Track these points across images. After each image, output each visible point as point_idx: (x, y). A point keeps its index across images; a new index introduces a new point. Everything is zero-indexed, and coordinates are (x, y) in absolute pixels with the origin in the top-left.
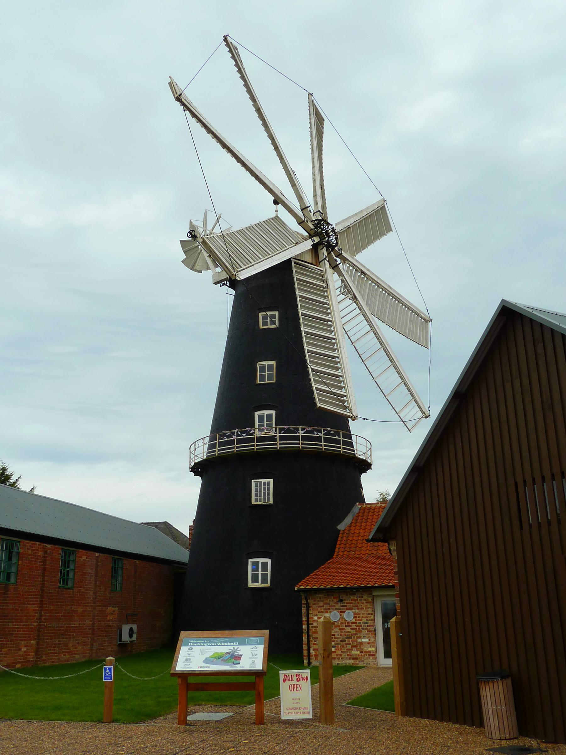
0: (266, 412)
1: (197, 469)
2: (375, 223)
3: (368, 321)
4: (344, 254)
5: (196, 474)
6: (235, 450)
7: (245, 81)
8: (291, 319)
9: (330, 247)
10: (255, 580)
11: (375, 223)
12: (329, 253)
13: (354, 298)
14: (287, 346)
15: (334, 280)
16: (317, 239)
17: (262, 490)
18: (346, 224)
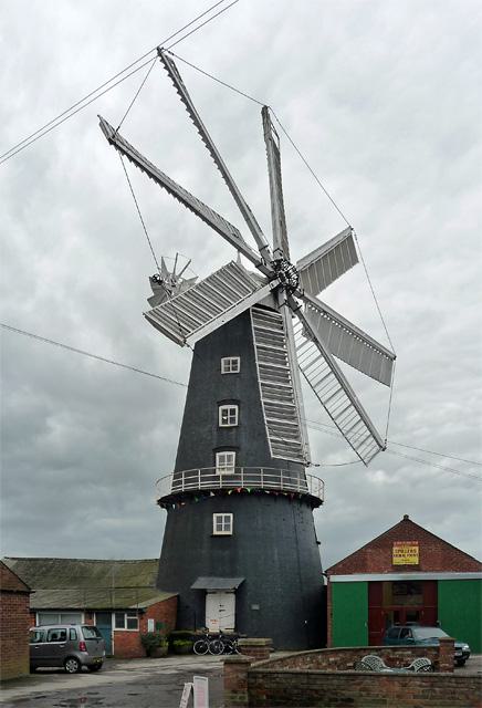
0: (226, 453)
1: (164, 502)
2: (340, 255)
3: (327, 359)
4: (306, 295)
5: (162, 507)
6: (200, 487)
7: (199, 127)
8: (251, 407)
9: (291, 289)
10: (219, 528)
11: (340, 255)
12: (289, 296)
13: (316, 341)
14: (245, 391)
15: (296, 325)
16: (275, 283)
17: (222, 523)
18: (308, 262)
